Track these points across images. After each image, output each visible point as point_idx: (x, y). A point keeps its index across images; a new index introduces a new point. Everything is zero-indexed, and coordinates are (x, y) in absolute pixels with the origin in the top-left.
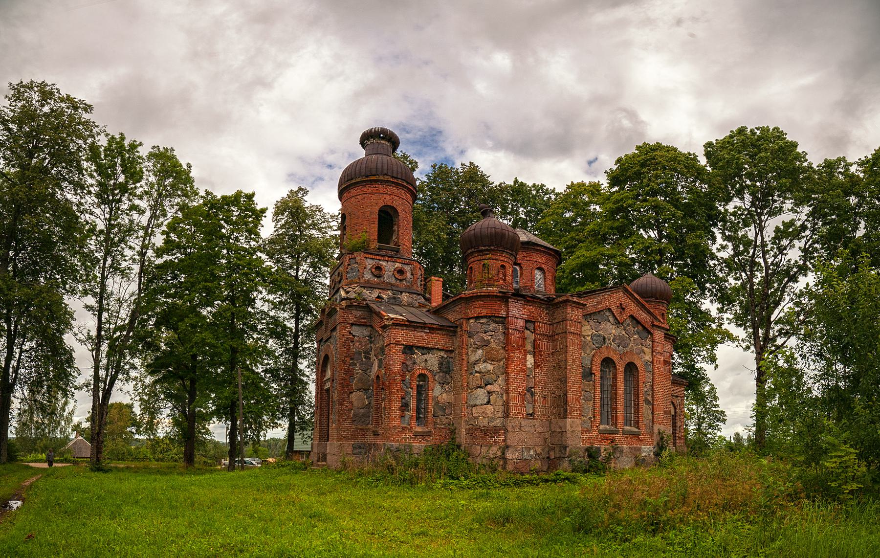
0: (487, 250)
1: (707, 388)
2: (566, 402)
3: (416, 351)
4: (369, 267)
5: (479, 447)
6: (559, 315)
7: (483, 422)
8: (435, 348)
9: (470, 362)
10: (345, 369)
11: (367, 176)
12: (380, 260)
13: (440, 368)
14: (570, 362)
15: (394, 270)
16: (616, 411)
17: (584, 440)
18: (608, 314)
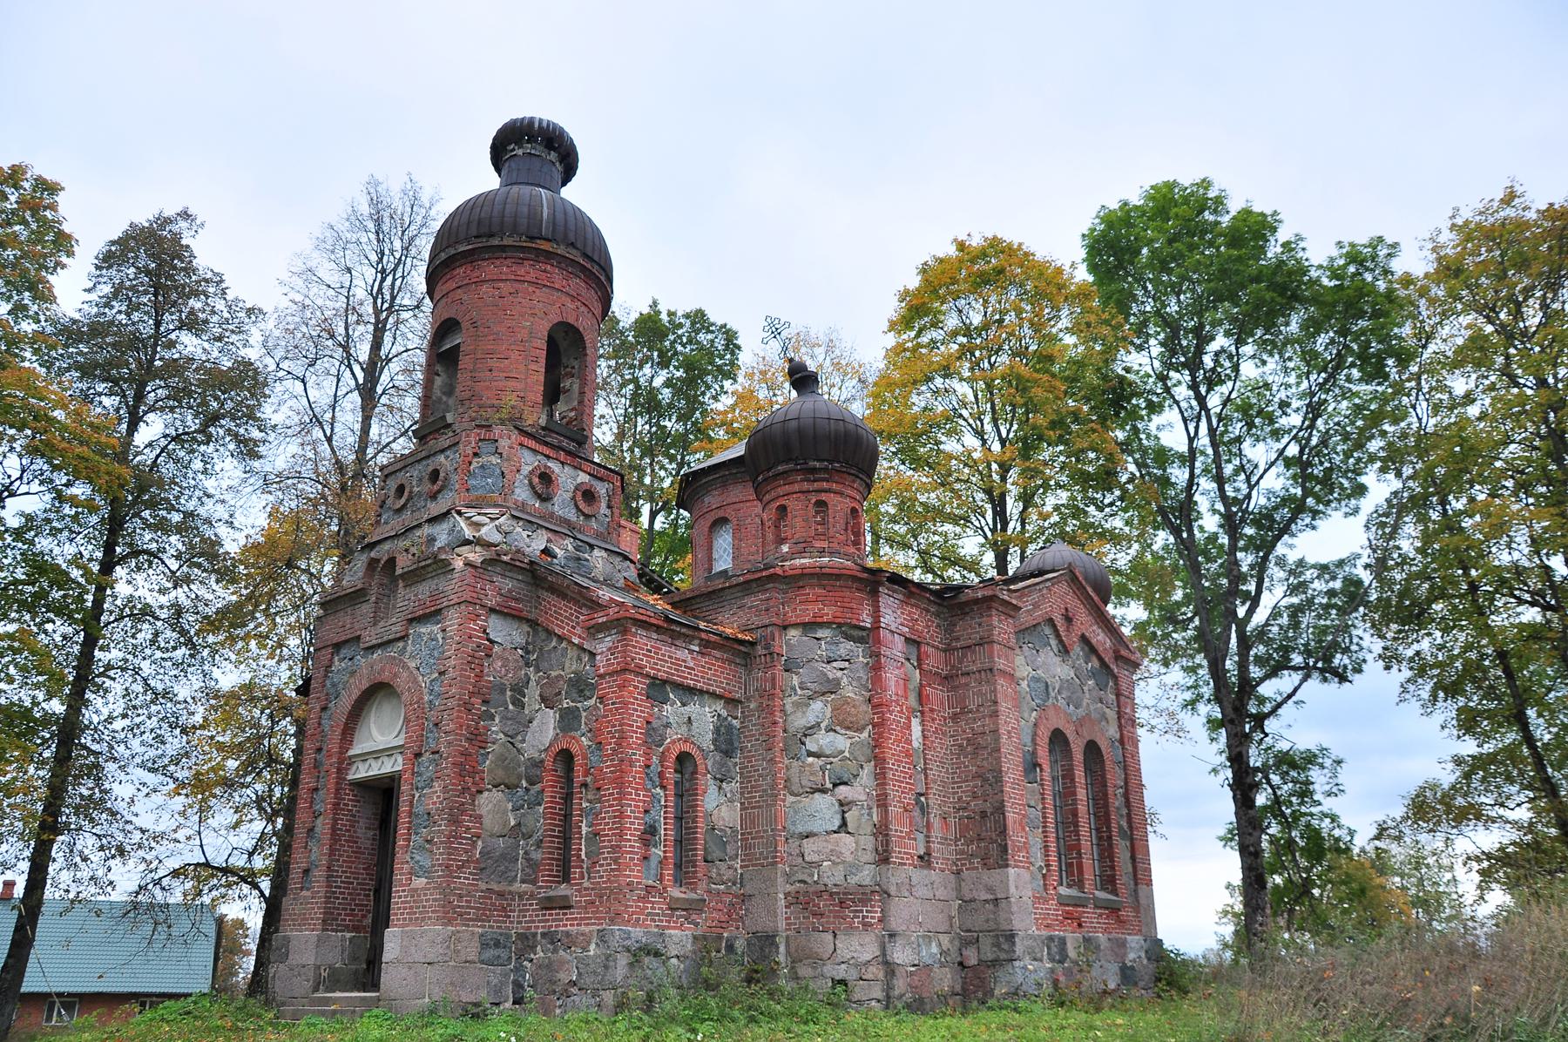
0: (825, 470)
4: (526, 470)
5: (829, 937)
6: (968, 630)
7: (832, 876)
8: (707, 692)
9: (791, 730)
10: (469, 726)
11: (532, 238)
12: (548, 457)
13: (714, 741)
15: (576, 488)
16: (1079, 853)
18: (1048, 630)
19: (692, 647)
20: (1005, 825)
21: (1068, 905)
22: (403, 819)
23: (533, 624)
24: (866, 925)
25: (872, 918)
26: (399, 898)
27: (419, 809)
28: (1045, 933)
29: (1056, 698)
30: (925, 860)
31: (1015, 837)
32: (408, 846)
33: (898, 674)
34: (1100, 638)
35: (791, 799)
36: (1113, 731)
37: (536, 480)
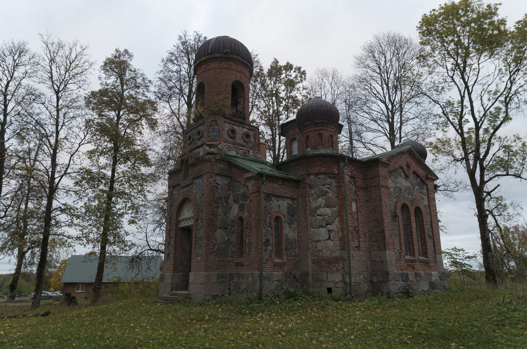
1: (107, 61)
2: (384, 238)
3: (273, 199)
4: (226, 129)
5: (325, 274)
7: (326, 254)
8: (285, 197)
10: (211, 211)
12: (233, 125)
13: (288, 212)
14: (384, 208)
15: (243, 134)
16: (413, 245)
17: (397, 267)
18: (400, 171)
19: (279, 183)
20: (385, 237)
21: (409, 262)
22: (194, 239)
23: (230, 177)
24: (338, 270)
25: (340, 267)
26: (193, 263)
27: (198, 236)
28: (400, 272)
29: (404, 193)
30: (358, 247)
31: (389, 240)
32: (195, 248)
33: (349, 188)
34: (421, 172)
35: (312, 229)
36: (426, 203)
37: (230, 132)
